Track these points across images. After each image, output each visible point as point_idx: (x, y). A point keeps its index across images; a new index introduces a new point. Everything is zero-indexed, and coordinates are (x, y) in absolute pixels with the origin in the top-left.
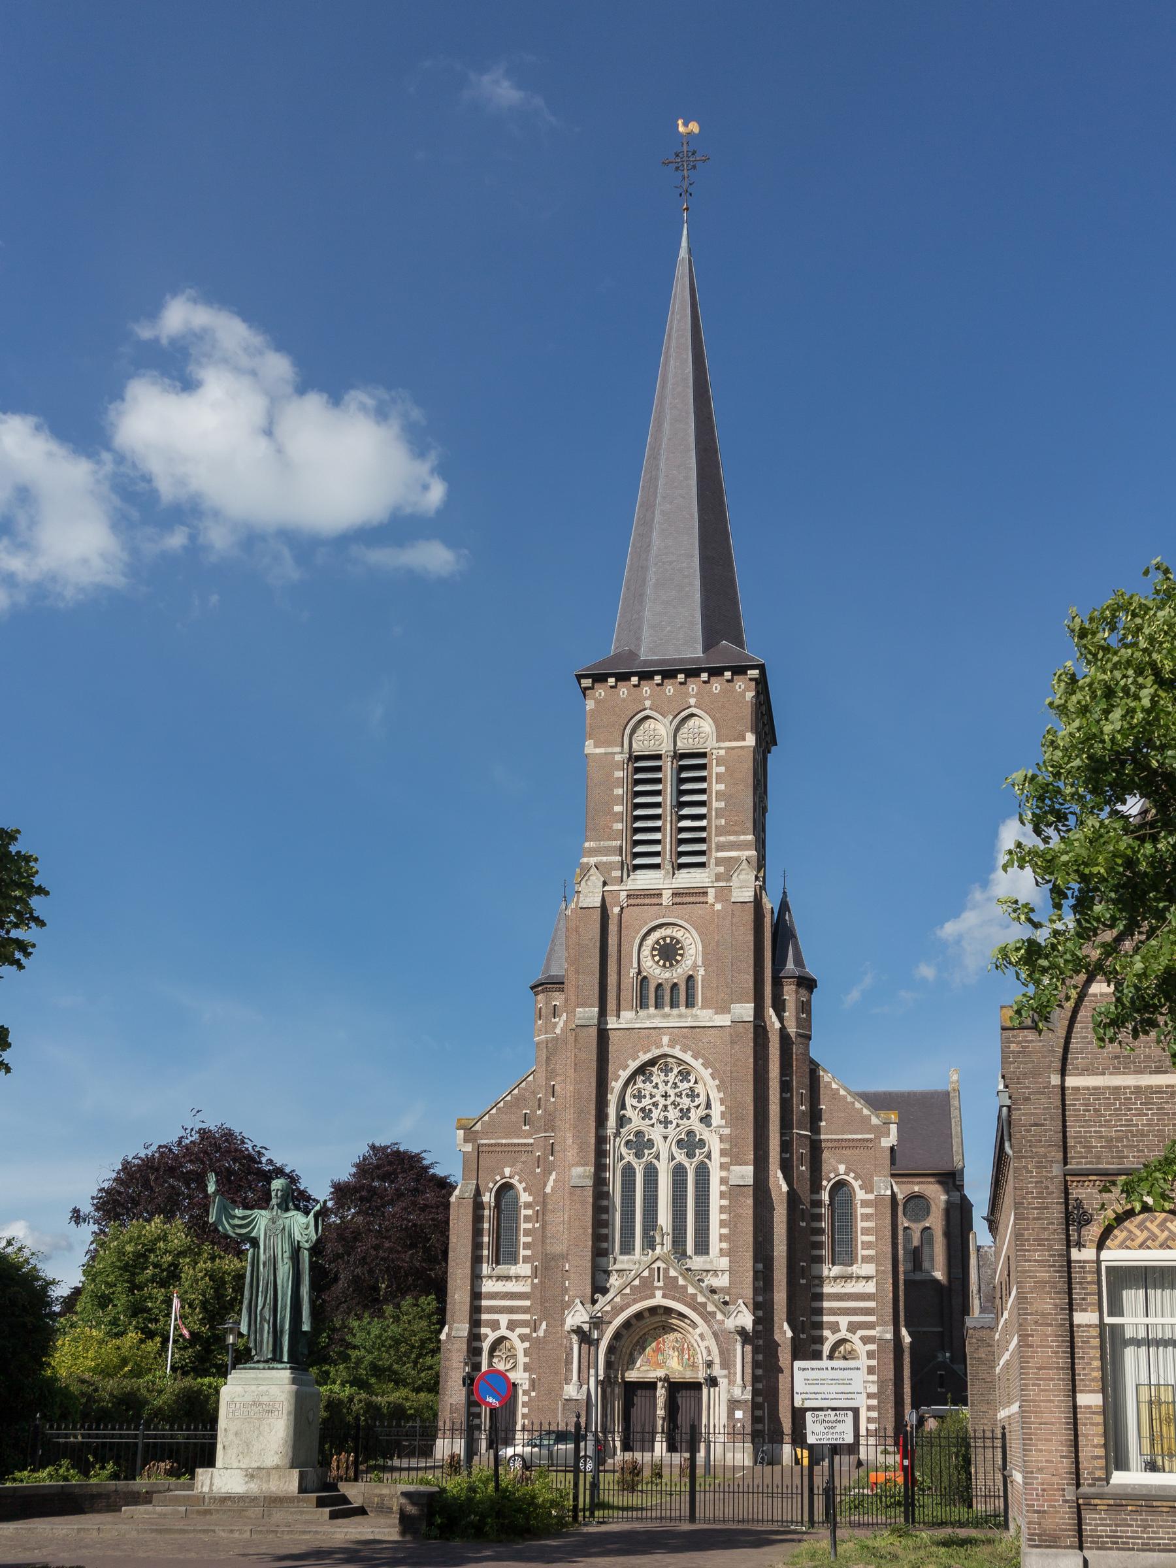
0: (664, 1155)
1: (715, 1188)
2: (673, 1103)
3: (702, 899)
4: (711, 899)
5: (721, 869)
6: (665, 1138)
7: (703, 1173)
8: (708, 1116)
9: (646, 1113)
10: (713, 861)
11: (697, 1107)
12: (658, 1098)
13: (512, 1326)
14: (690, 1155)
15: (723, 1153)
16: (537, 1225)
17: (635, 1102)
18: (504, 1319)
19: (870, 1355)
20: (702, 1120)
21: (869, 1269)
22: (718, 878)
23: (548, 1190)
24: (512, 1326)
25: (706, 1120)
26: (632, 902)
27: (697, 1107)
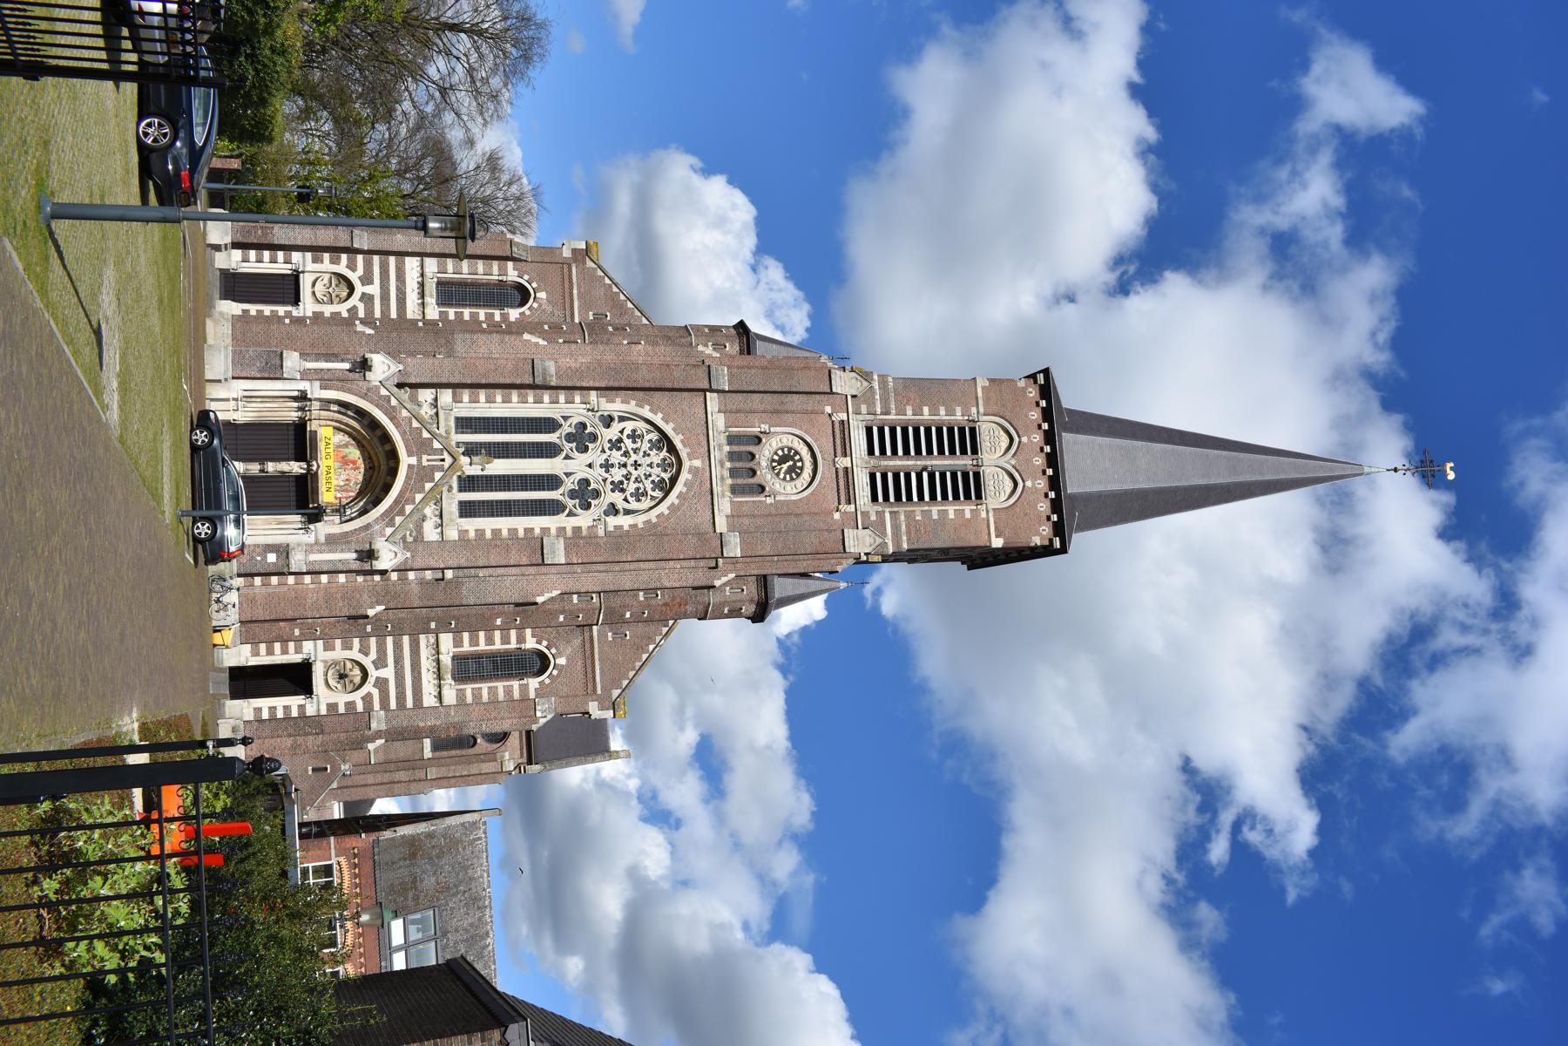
4: (843, 507)
6: (590, 466)
7: (553, 508)
9: (616, 444)
11: (626, 500)
12: (634, 457)
13: (381, 684)
15: (577, 530)
17: (627, 432)
20: (613, 505)
21: (450, 696)
22: (865, 514)
23: (526, 336)
24: (381, 684)
25: (613, 510)
26: (837, 426)
27: (626, 500)
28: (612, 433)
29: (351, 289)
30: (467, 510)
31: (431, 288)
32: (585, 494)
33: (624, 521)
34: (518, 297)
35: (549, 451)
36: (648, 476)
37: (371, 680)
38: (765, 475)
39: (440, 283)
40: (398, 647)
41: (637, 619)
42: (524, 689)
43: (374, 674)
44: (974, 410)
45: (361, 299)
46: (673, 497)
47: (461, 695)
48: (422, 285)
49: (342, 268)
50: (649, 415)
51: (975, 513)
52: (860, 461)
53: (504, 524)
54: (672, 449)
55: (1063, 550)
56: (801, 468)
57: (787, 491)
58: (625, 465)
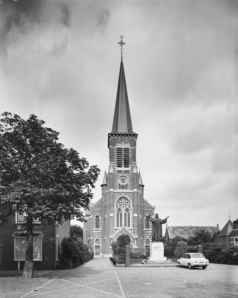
0: (123, 212)
1: (131, 217)
2: (123, 204)
3: (121, 172)
4: (130, 172)
5: (131, 168)
6: (123, 209)
7: (129, 214)
8: (130, 206)
9: (120, 205)
10: (130, 166)
11: (128, 205)
12: (122, 203)
13: (99, 237)
14: (127, 212)
15: (132, 212)
16: (103, 222)
18: (148, 237)
19: (101, 241)
20: (129, 206)
21: (101, 229)
22: (131, 169)
24: (99, 237)
25: (129, 206)
26: (125, 172)
27: (128, 205)
28: (119, 206)
29: (97, 239)
30: (129, 226)
31: (97, 229)
32: (127, 210)
33: (131, 205)
34: (97, 217)
35: (121, 215)
36: (123, 201)
37: (148, 239)
38: (125, 184)
39: (96, 228)
40: (145, 235)
41: (143, 204)
42: (101, 219)
43: (147, 238)
44: (115, 148)
45: (99, 238)
46: (128, 198)
47: (101, 227)
48: (97, 230)
49: (95, 240)
50: (117, 200)
51: (131, 150)
52: (123, 169)
53: (116, 221)
54: (121, 198)
55: (109, 134)
56: (124, 178)
57: (127, 182)
58: (123, 204)
